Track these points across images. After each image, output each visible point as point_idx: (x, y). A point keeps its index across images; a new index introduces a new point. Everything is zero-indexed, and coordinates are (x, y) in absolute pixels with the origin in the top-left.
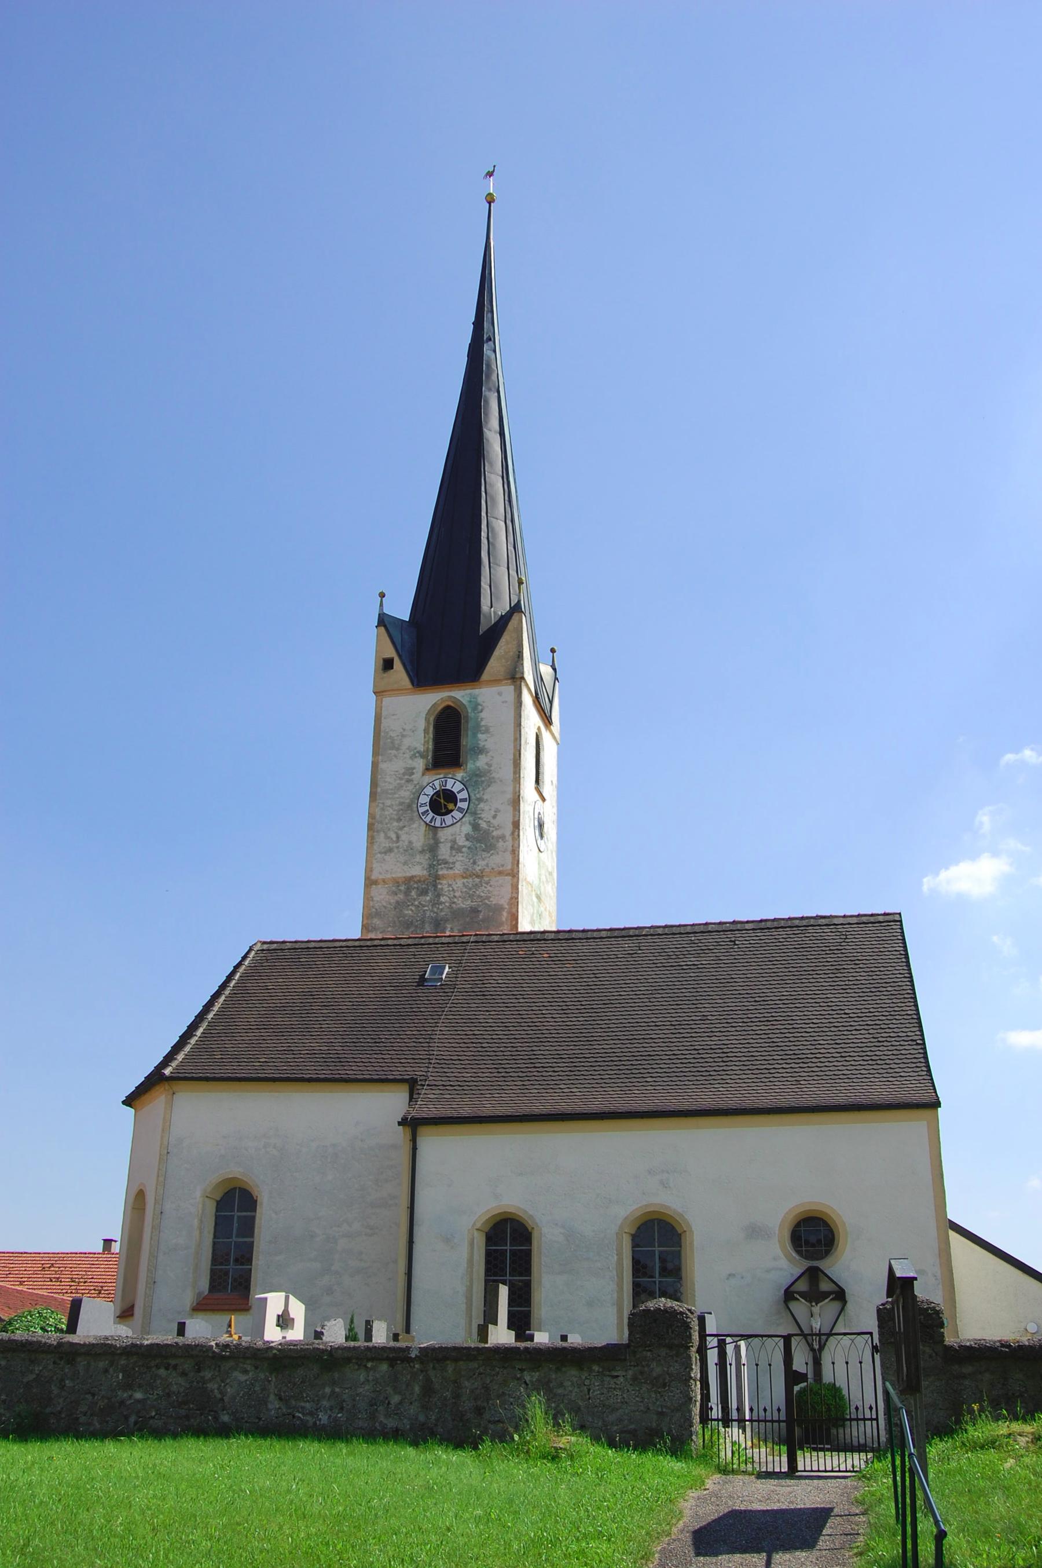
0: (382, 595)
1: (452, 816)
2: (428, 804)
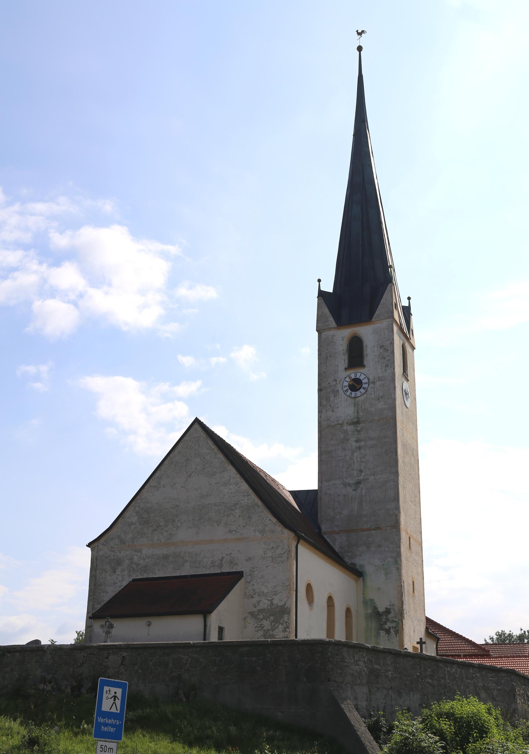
0: (319, 281)
1: (360, 392)
2: (348, 386)
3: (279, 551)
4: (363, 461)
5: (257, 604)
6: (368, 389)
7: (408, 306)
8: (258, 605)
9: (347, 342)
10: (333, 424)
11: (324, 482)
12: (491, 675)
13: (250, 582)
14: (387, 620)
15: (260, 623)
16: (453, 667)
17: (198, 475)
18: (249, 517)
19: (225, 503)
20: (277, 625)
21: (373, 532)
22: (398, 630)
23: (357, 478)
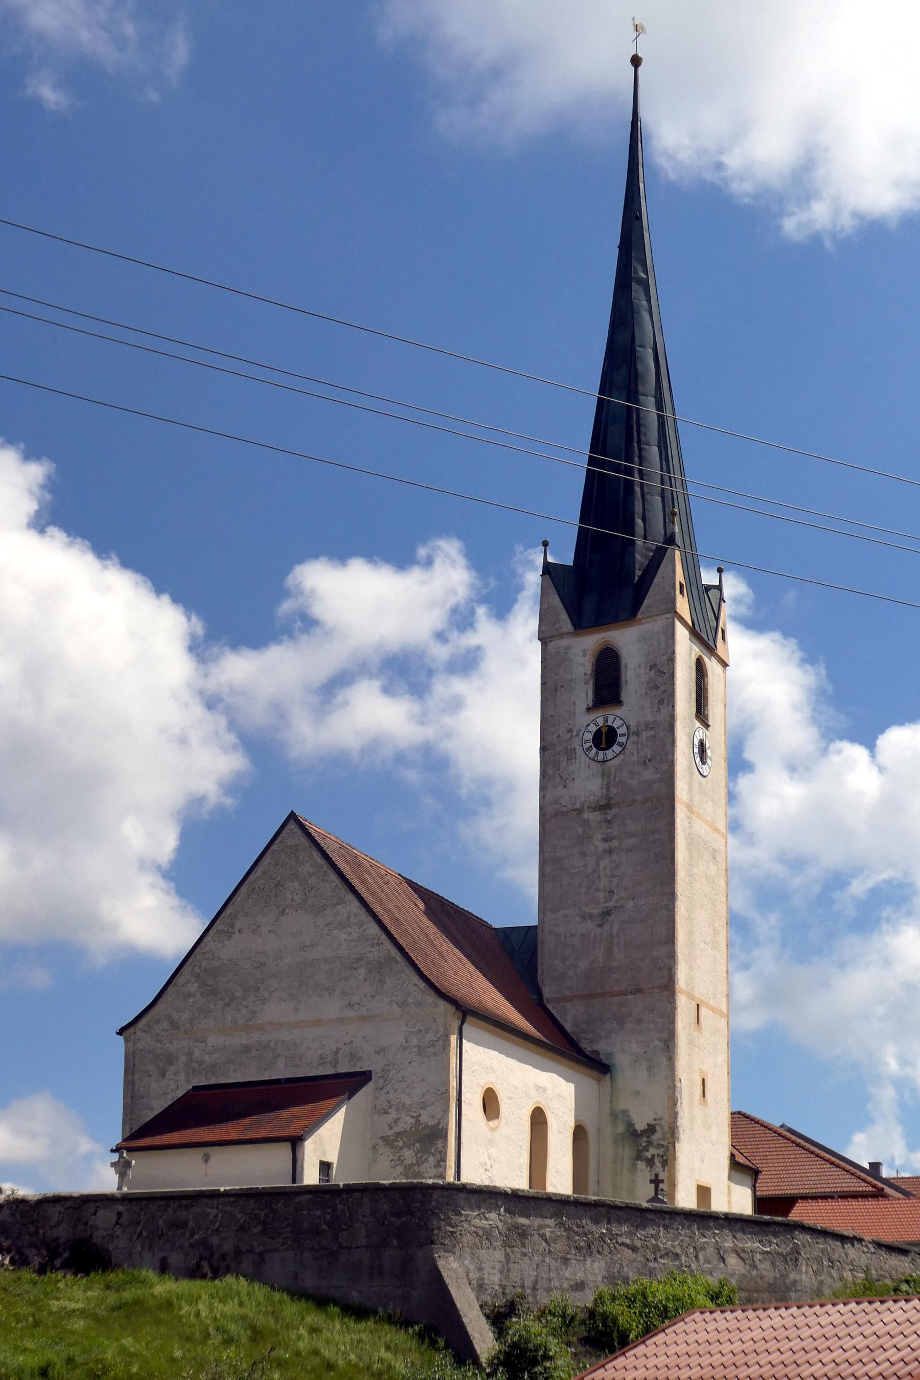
3: (430, 1036)
4: (615, 875)
5: (394, 1123)
6: (627, 745)
7: (718, 584)
8: (395, 1124)
9: (592, 660)
10: (565, 809)
11: (549, 913)
12: (751, 1230)
13: (383, 1088)
14: (650, 1143)
15: (399, 1154)
16: (674, 1219)
17: (297, 911)
18: (381, 981)
19: (341, 957)
20: (425, 1157)
21: (631, 997)
22: (667, 1160)
23: (605, 905)
